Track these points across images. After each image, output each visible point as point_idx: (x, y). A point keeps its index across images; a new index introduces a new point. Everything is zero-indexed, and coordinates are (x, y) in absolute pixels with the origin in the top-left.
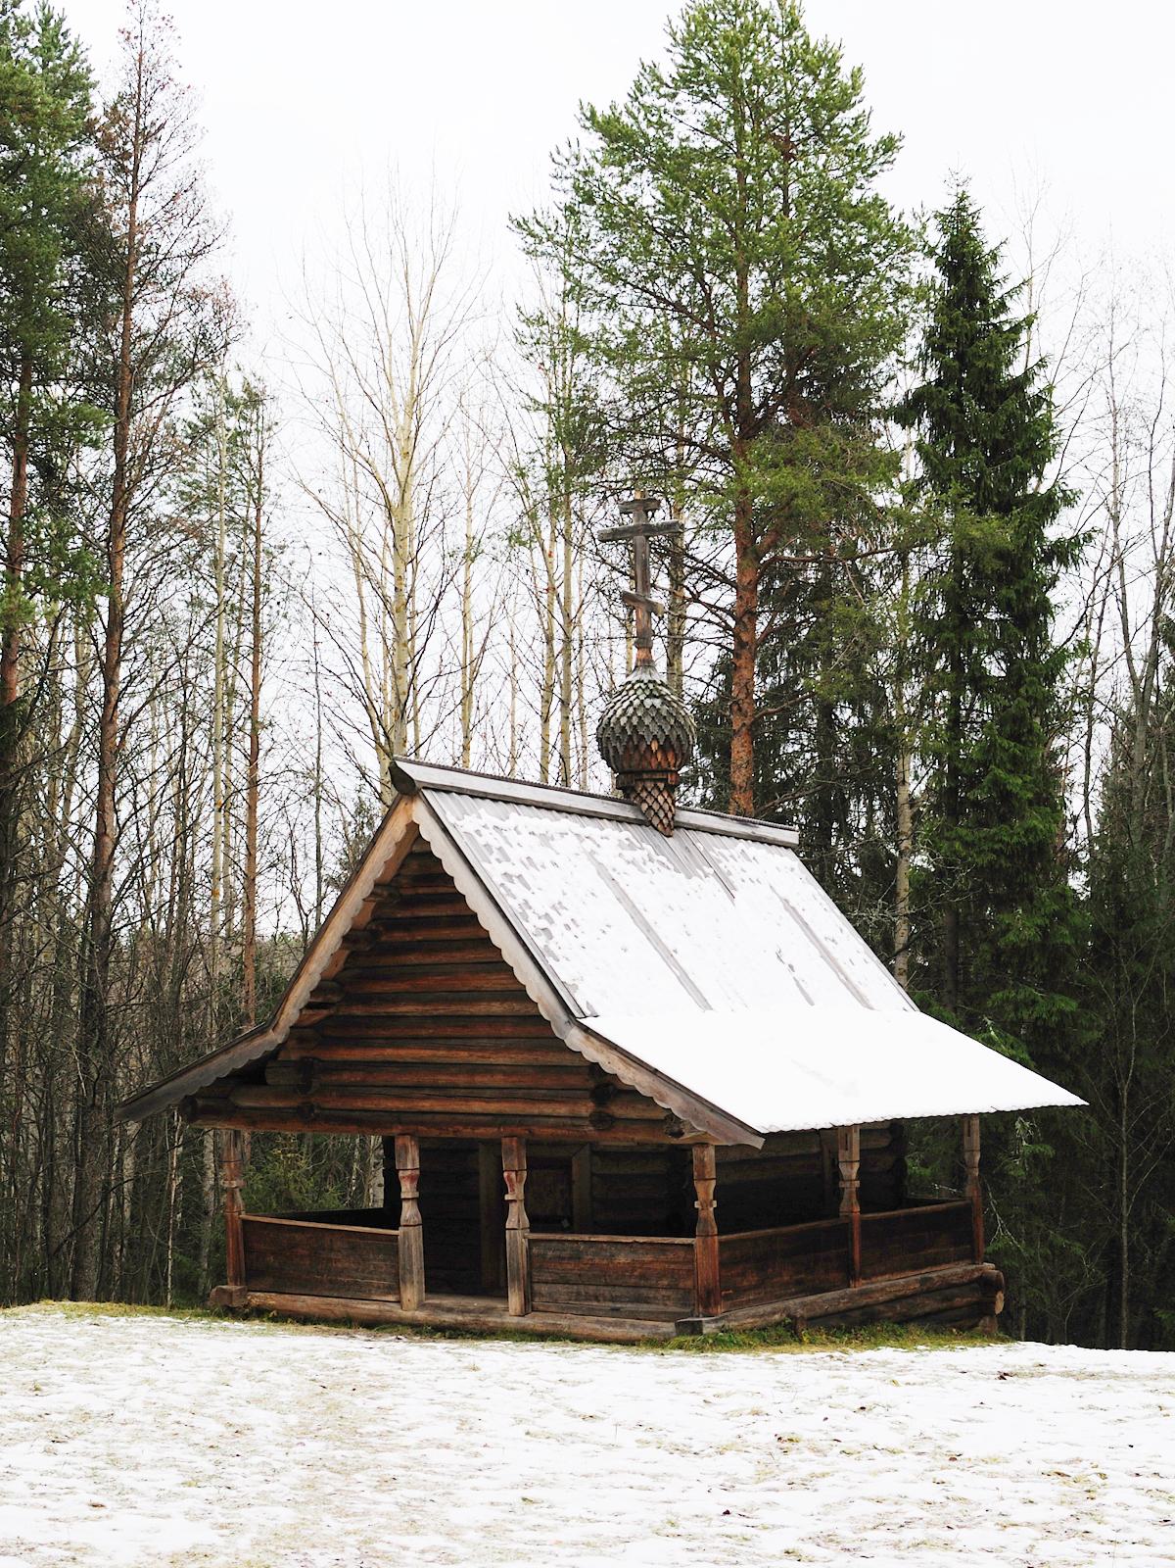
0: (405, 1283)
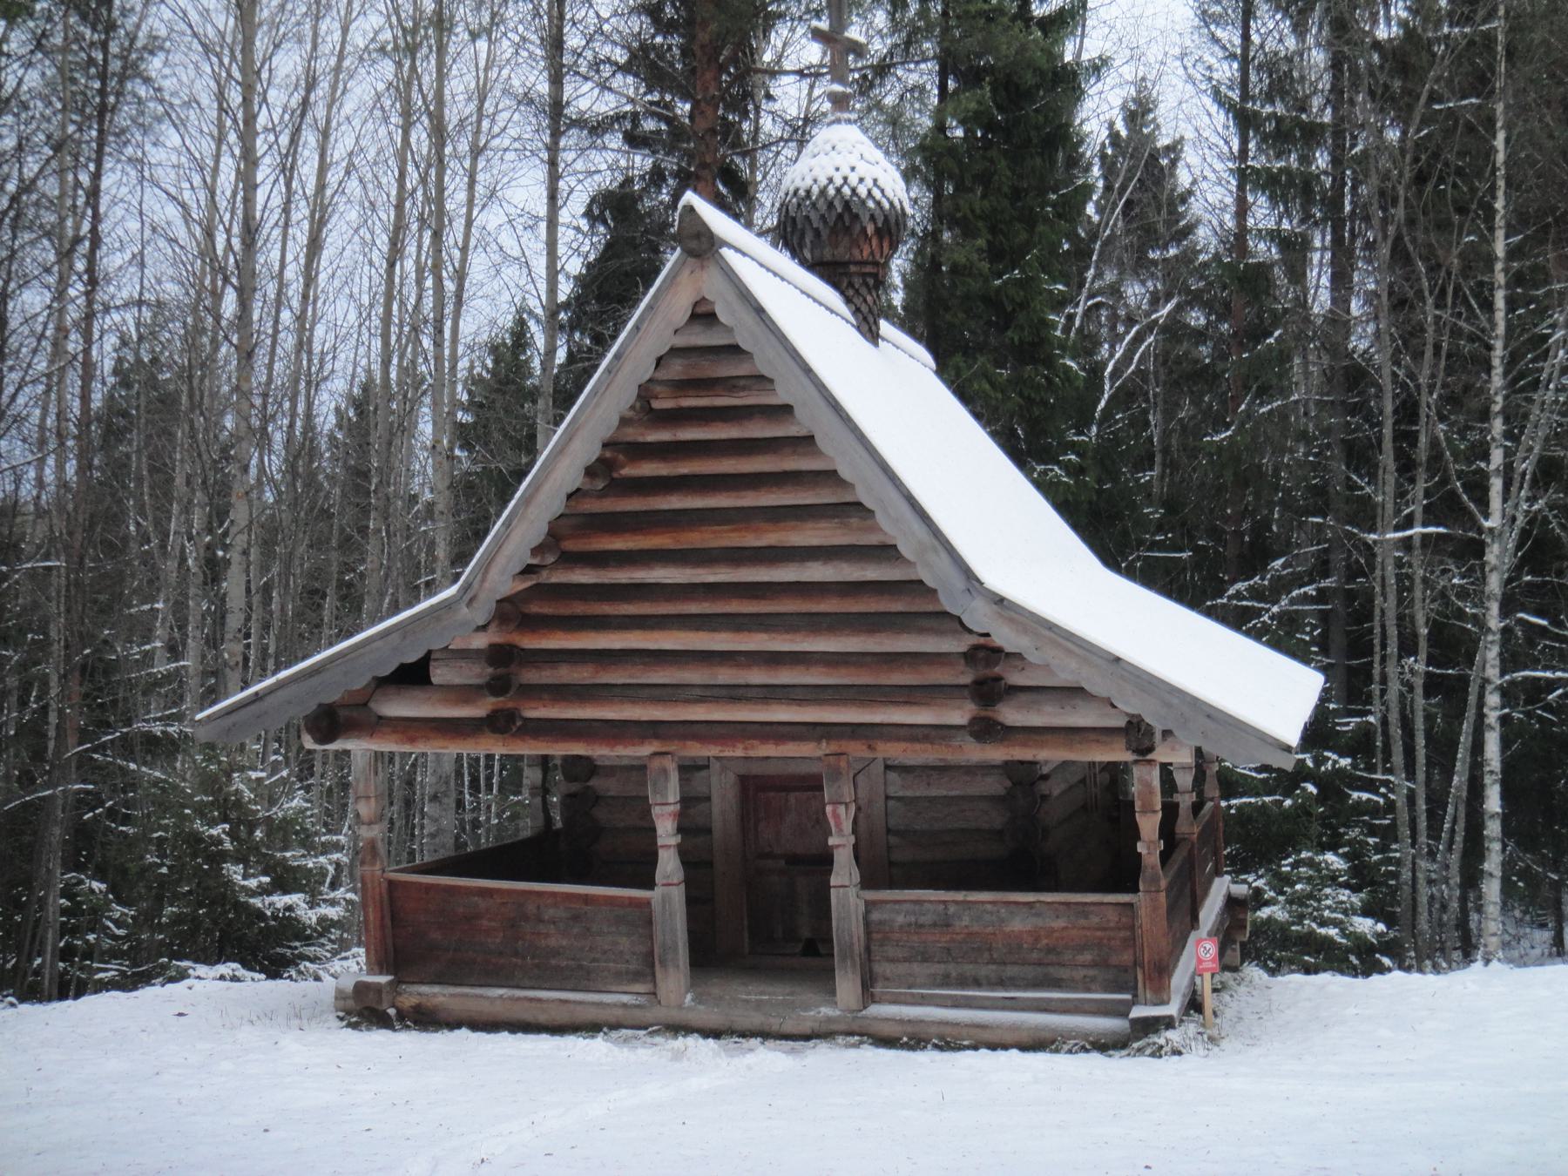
0: (663, 963)
